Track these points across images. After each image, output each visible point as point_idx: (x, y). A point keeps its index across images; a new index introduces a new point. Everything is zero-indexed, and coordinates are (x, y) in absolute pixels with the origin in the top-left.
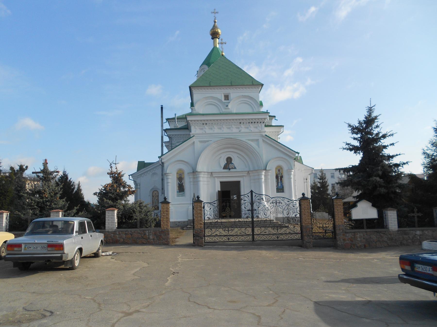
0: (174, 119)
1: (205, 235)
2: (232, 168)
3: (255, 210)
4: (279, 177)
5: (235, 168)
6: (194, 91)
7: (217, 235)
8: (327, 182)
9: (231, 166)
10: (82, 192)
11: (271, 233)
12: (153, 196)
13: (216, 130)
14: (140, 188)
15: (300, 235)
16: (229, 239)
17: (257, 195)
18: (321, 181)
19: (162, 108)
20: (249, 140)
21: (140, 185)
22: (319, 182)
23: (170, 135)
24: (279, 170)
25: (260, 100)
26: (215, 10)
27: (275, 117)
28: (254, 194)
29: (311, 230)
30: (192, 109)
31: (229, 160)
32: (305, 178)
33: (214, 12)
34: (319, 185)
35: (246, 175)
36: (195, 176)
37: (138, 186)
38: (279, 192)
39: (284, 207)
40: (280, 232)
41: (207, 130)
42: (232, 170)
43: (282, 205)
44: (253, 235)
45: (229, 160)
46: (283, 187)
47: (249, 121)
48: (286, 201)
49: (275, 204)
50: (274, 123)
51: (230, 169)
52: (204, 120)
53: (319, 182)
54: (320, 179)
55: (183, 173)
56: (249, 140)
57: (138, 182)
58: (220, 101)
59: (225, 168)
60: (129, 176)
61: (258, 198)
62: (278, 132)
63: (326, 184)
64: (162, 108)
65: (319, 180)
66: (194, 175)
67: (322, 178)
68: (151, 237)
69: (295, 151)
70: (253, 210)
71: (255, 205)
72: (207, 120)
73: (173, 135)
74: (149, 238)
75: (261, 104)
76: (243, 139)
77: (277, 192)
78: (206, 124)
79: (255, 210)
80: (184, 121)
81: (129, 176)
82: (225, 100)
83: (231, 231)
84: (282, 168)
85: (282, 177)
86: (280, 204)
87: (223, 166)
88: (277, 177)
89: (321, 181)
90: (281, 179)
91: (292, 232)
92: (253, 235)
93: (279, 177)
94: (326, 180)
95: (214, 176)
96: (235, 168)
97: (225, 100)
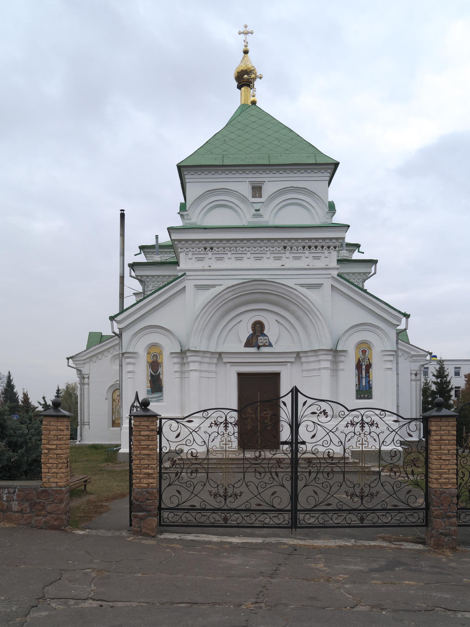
0: (152, 247)
1: (163, 506)
2: (264, 346)
3: (304, 443)
4: (364, 367)
5: (270, 345)
6: (188, 178)
7: (193, 508)
8: (449, 382)
9: (261, 340)
10: (15, 390)
11: (345, 507)
12: (113, 400)
13: (230, 262)
14: (88, 384)
15: (422, 514)
16: (362, 520)
17: (310, 402)
18: (439, 380)
19: (122, 216)
20: (302, 285)
21: (88, 378)
22: (435, 383)
23: (142, 276)
24: (364, 352)
25: (330, 200)
26: (246, 27)
27: (358, 246)
28: (301, 399)
29: (455, 500)
30: (182, 216)
31: (258, 327)
32: (414, 372)
33: (243, 33)
34: (434, 388)
35: (293, 360)
36: (185, 361)
37: (86, 381)
38: (361, 398)
39: (382, 437)
40: (369, 506)
41: (210, 261)
42: (263, 349)
43: (378, 431)
44: (294, 511)
45: (258, 327)
46: (371, 388)
47: (303, 244)
48: (390, 419)
49: (358, 428)
50: (356, 256)
51: (259, 347)
52: (207, 240)
53: (435, 383)
54: (437, 377)
55: (161, 353)
56: (302, 285)
57: (85, 370)
58: (243, 199)
59: (248, 344)
60: (68, 359)
61: (314, 409)
62: (365, 273)
63: (448, 386)
64: (122, 216)
65: (434, 379)
66: (183, 358)
67: (441, 374)
68: (15, 506)
69: (399, 312)
70: (297, 443)
71: (302, 429)
72: (211, 242)
73: (148, 276)
74: (9, 509)
75: (332, 207)
76: (290, 283)
77: (357, 398)
78: (212, 248)
79: (304, 443)
80: (170, 252)
81: (68, 359)
82: (254, 196)
83: (231, 499)
84: (370, 349)
85: (369, 366)
86: (374, 428)
87: (244, 341)
88: (359, 366)
89: (439, 380)
90: (368, 372)
91: (402, 506)
92: (294, 511)
93: (364, 367)
94: (448, 379)
95: (225, 360)
96: (270, 345)
97: (254, 196)
